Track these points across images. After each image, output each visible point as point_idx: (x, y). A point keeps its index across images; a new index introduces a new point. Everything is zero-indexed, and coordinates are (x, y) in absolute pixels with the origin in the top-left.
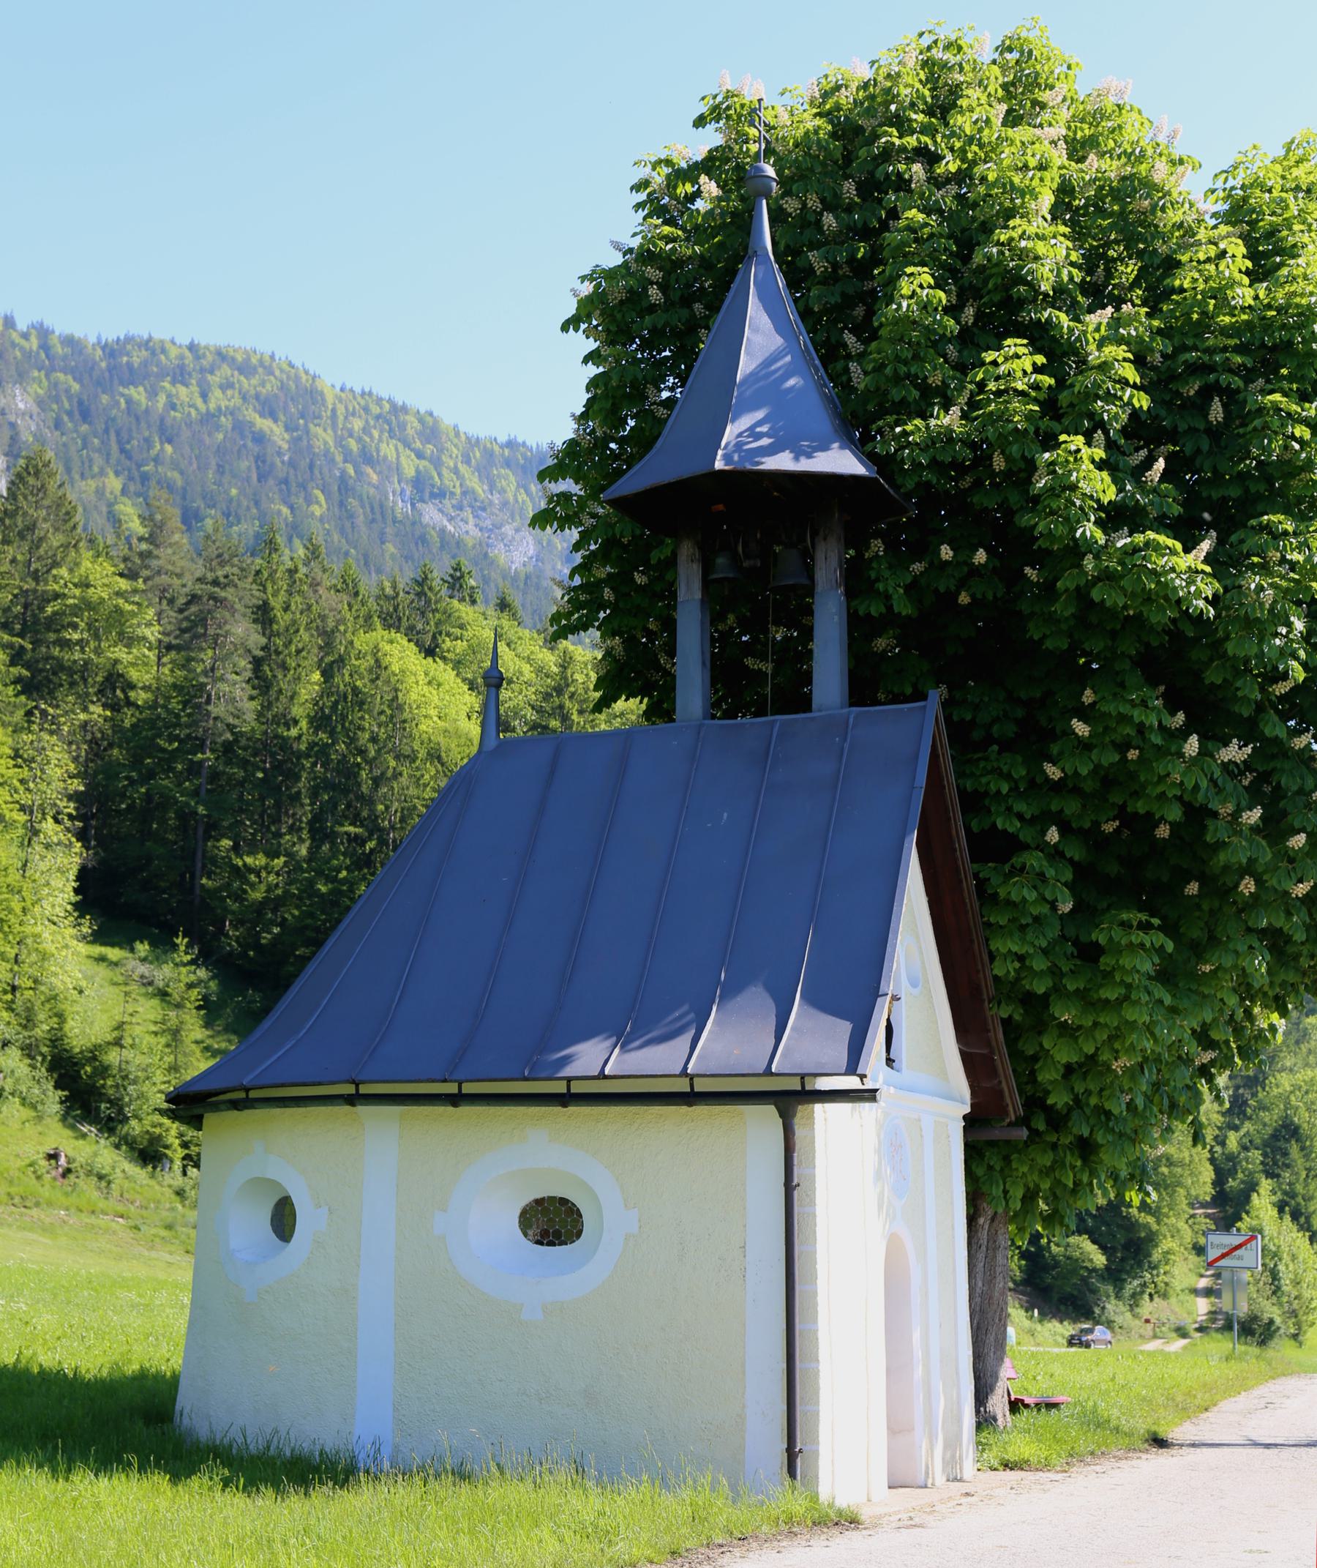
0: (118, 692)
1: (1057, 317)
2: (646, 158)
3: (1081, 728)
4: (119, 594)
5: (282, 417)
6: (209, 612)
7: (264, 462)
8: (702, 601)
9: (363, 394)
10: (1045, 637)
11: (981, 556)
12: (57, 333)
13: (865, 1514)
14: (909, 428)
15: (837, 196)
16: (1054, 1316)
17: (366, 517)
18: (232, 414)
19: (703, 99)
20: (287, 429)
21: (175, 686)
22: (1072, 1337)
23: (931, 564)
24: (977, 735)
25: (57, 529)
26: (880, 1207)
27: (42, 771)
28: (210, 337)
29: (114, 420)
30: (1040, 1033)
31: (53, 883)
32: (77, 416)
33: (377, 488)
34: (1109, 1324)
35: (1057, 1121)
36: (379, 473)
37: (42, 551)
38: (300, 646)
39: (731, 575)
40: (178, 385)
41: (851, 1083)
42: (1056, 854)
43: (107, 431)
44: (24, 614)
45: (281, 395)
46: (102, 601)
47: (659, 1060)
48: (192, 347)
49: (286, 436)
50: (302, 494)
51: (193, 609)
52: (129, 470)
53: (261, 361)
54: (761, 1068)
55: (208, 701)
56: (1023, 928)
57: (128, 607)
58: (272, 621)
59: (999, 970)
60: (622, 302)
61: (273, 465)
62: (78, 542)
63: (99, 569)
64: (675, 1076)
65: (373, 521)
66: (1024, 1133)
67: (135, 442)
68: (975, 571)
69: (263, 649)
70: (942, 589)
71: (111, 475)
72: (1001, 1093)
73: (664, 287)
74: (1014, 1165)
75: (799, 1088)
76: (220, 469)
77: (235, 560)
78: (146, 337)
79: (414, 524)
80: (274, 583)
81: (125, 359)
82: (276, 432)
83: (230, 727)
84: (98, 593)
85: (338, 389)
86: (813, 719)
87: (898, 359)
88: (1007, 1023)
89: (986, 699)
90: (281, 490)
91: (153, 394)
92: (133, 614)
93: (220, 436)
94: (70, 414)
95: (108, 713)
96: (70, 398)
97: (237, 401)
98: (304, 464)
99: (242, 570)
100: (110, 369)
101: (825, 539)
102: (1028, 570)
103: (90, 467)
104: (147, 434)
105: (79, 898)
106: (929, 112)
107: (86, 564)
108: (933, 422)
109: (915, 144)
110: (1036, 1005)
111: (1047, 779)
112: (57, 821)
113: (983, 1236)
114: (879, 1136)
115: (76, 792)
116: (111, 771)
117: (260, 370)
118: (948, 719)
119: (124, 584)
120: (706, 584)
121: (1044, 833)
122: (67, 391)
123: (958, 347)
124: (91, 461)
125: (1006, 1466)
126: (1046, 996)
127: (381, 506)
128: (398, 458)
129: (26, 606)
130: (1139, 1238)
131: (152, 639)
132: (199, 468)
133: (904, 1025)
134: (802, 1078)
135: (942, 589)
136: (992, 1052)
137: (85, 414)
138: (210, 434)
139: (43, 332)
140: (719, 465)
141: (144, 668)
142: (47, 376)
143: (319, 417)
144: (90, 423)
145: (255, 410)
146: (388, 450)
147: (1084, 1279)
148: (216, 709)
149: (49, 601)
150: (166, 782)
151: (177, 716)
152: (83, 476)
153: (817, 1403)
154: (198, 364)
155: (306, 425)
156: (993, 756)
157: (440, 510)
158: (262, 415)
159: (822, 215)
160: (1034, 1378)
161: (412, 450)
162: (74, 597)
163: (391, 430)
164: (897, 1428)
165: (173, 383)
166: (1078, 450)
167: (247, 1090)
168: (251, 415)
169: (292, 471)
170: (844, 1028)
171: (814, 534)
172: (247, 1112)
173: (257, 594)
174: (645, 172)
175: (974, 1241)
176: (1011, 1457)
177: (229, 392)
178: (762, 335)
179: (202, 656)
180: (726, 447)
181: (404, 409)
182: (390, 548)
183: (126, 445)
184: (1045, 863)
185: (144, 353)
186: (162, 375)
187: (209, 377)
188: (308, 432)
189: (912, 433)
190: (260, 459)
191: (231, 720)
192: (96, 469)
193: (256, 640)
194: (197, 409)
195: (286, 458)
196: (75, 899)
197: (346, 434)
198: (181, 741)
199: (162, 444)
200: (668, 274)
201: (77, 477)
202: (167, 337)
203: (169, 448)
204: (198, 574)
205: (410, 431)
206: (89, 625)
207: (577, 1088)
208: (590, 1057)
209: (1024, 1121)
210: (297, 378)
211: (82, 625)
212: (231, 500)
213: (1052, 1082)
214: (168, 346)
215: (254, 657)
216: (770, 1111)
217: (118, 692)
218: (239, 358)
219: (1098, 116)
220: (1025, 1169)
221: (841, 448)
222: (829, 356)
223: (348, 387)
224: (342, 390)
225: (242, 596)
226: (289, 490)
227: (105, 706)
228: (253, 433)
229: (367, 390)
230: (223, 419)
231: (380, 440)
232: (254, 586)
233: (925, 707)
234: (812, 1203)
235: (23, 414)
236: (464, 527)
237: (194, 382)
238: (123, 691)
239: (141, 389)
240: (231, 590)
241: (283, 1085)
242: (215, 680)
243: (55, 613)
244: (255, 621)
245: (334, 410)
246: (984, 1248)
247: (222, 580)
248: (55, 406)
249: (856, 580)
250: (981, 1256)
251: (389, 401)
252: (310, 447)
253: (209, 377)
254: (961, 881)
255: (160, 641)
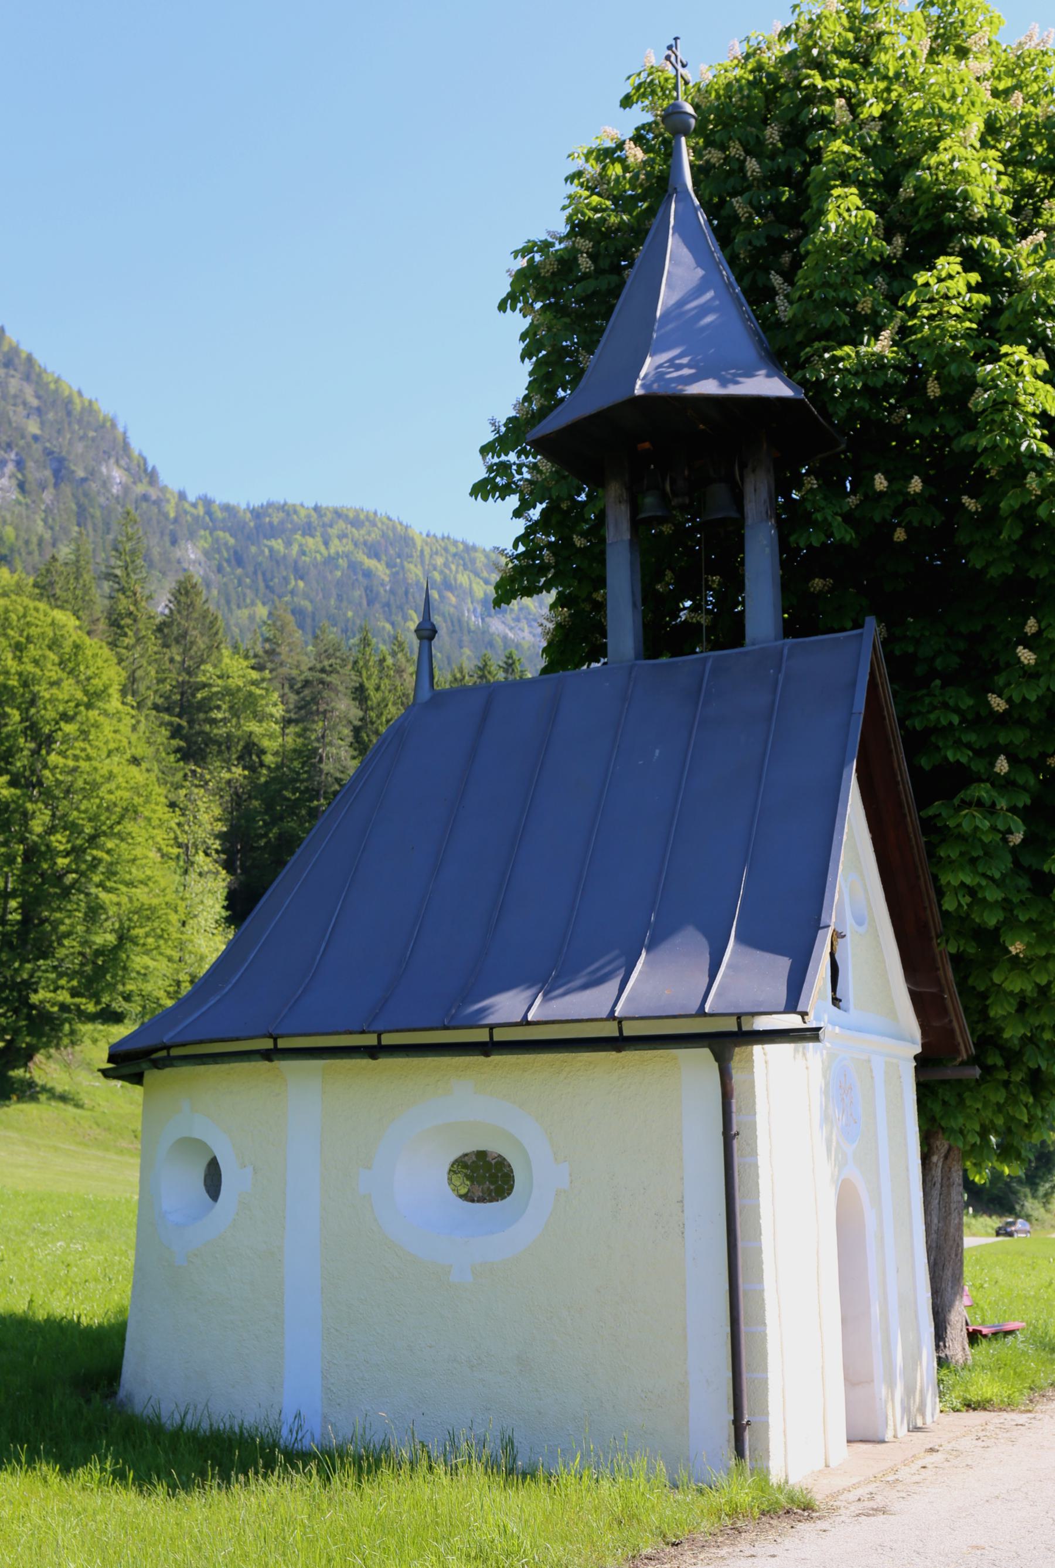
0: (254, 757)
1: (990, 244)
2: (579, 150)
3: (1027, 656)
4: (254, 683)
5: (384, 558)
6: (319, 693)
7: (371, 591)
8: (631, 541)
9: (443, 538)
10: (988, 565)
11: (916, 484)
12: (217, 502)
13: (818, 1497)
14: (838, 353)
15: (760, 142)
16: (985, 1212)
17: (448, 629)
18: (347, 556)
19: (629, 78)
20: (388, 566)
21: (295, 751)
22: (1000, 1228)
23: (866, 496)
24: (920, 670)
25: (202, 635)
26: (829, 1150)
27: (195, 817)
28: (329, 502)
29: (260, 564)
30: (990, 970)
31: (205, 901)
32: (233, 562)
33: (455, 607)
34: (1028, 1218)
35: (1012, 1058)
36: (457, 597)
37: (192, 652)
38: (389, 717)
39: (659, 514)
40: (307, 537)
41: (792, 1021)
42: (1006, 784)
43: (255, 573)
44: (181, 700)
45: (382, 541)
46: (239, 689)
47: (585, 1005)
48: (316, 509)
49: (388, 572)
50: (400, 614)
51: (307, 692)
52: (273, 602)
53: (367, 517)
54: (693, 1008)
55: (321, 761)
56: (973, 861)
57: (258, 692)
58: (367, 698)
59: (949, 905)
60: (553, 273)
61: (378, 593)
62: (219, 644)
63: (235, 663)
64: (601, 1020)
65: (453, 631)
66: (977, 1072)
67: (276, 580)
68: (911, 501)
69: (361, 720)
70: (877, 519)
71: (260, 605)
72: (952, 1031)
73: (593, 257)
74: (968, 1103)
75: (736, 1029)
76: (340, 598)
77: (338, 654)
78: (282, 502)
79: (483, 633)
80: (368, 670)
81: (267, 519)
82: (379, 568)
83: (338, 780)
84: (236, 682)
85: (424, 534)
86: (746, 653)
87: (826, 284)
88: (957, 960)
89: (927, 633)
90: (384, 612)
91: (288, 544)
92: (262, 697)
93: (339, 573)
94: (228, 561)
95: (246, 773)
96: (228, 549)
97: (350, 547)
98: (401, 591)
99: (343, 660)
100: (257, 527)
101: (754, 471)
102: (965, 499)
103: (244, 600)
104: (285, 574)
105: (228, 913)
106: (854, 58)
107: (226, 660)
108: (863, 349)
109: (839, 86)
110: (990, 940)
111: (992, 712)
112: (207, 855)
113: (937, 1173)
114: (824, 1076)
115: (220, 832)
116: (249, 817)
117: (367, 524)
118: (889, 657)
119: (255, 675)
120: (636, 524)
121: (992, 764)
122: (226, 544)
123: (887, 280)
124: (244, 595)
125: (969, 1406)
126: (997, 929)
127: (459, 621)
128: (471, 584)
129: (182, 694)
130: (1049, 1152)
131: (278, 715)
132: (324, 597)
133: (850, 968)
134: (739, 1018)
135: (877, 519)
136: (942, 991)
137: (238, 560)
138: (331, 572)
139: (207, 502)
140: (638, 391)
141: (271, 736)
142: (211, 534)
143: (412, 556)
144: (243, 568)
145: (364, 553)
146: (463, 579)
147: (1007, 1184)
148: (327, 767)
149: (198, 690)
150: (291, 824)
151: (298, 774)
152: (239, 607)
153: (765, 1370)
154: (321, 521)
155: (402, 562)
156: (937, 692)
157: (503, 622)
158: (369, 557)
159: (745, 160)
160: (982, 1286)
161: (481, 578)
162: (218, 686)
163: (465, 565)
164: (855, 1379)
165: (303, 535)
166: (1020, 362)
167: (168, 1048)
168: (362, 557)
169: (392, 598)
170: (783, 964)
171: (743, 466)
172: (167, 1071)
173: (355, 678)
174: (579, 163)
175: (929, 1178)
176: (974, 1396)
177: (344, 541)
178: (682, 271)
179: (314, 726)
180: (646, 375)
181: (474, 548)
182: (467, 651)
183: (267, 579)
184: (994, 794)
185: (281, 515)
186: (294, 530)
187: (329, 530)
188: (403, 568)
189: (842, 359)
190: (368, 589)
191: (338, 775)
192: (248, 601)
193: (355, 713)
194: (321, 554)
195: (388, 588)
196: (225, 913)
197: (431, 568)
198: (301, 792)
199: (296, 579)
200: (597, 244)
201: (234, 607)
202: (297, 502)
203: (301, 584)
204: (310, 665)
205: (479, 565)
206: (231, 708)
207: (500, 1035)
208: (508, 1006)
209: (975, 1060)
210: (394, 528)
211: (225, 707)
212: (348, 620)
213: (1004, 1017)
214: (298, 508)
215: (354, 727)
216: (703, 1056)
217: (254, 757)
218: (351, 515)
219: (1022, 62)
220: (979, 1106)
221: (768, 376)
222: (757, 295)
223: (432, 533)
224: (428, 535)
225: (343, 680)
226: (390, 611)
227: (244, 768)
228: (363, 570)
229: (446, 535)
230: (340, 560)
231: (457, 572)
232: (352, 673)
233: (861, 634)
234: (754, 1153)
235: (194, 562)
236: (522, 635)
237: (318, 534)
238: (259, 757)
239: (280, 541)
240: (334, 676)
241: (201, 1042)
242: (325, 746)
243: (204, 699)
244: (354, 699)
245: (422, 551)
246: (938, 1185)
247: (328, 668)
248: (217, 556)
249: (790, 521)
250: (935, 1193)
251: (463, 542)
252: (405, 579)
253: (329, 530)
254: (905, 816)
255: (284, 717)
